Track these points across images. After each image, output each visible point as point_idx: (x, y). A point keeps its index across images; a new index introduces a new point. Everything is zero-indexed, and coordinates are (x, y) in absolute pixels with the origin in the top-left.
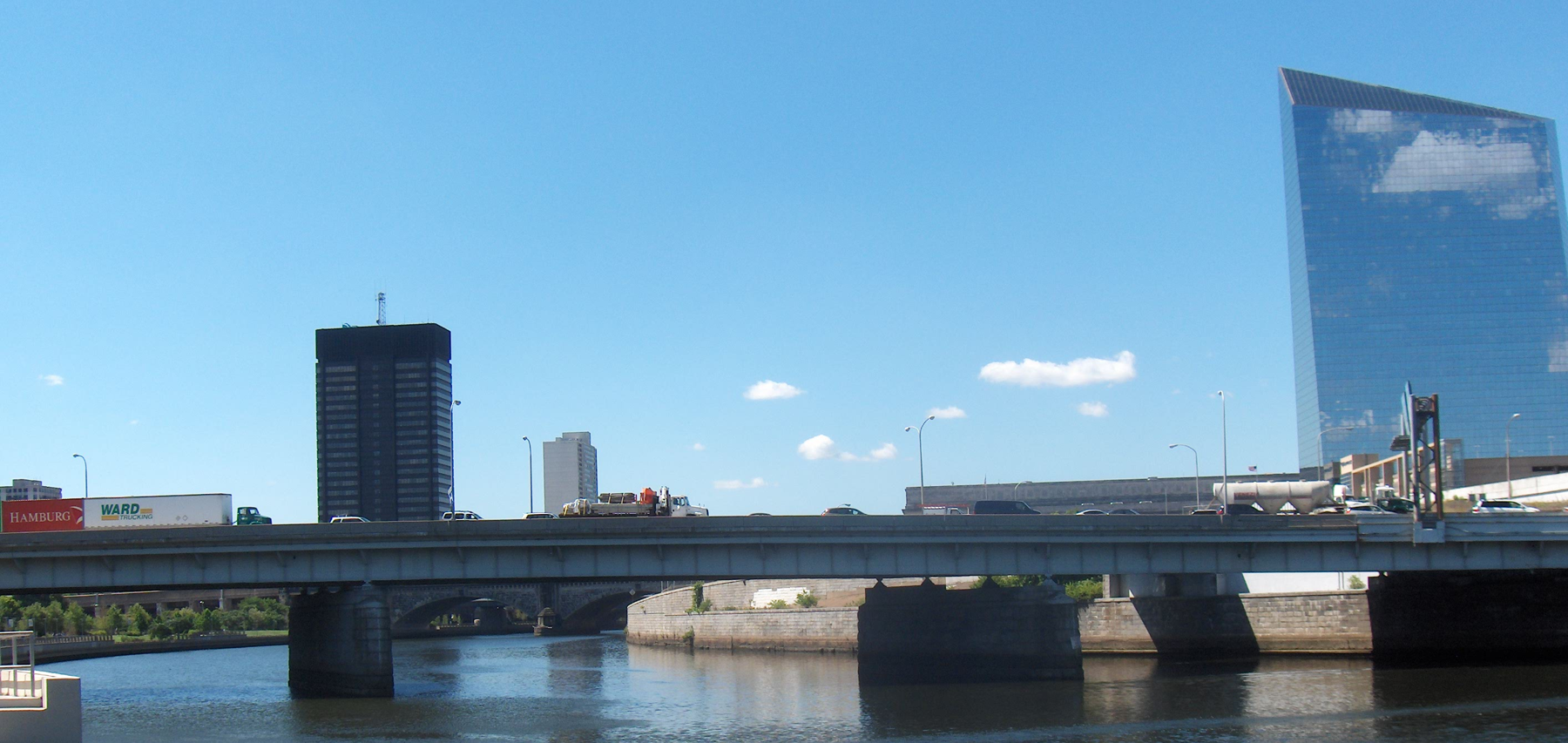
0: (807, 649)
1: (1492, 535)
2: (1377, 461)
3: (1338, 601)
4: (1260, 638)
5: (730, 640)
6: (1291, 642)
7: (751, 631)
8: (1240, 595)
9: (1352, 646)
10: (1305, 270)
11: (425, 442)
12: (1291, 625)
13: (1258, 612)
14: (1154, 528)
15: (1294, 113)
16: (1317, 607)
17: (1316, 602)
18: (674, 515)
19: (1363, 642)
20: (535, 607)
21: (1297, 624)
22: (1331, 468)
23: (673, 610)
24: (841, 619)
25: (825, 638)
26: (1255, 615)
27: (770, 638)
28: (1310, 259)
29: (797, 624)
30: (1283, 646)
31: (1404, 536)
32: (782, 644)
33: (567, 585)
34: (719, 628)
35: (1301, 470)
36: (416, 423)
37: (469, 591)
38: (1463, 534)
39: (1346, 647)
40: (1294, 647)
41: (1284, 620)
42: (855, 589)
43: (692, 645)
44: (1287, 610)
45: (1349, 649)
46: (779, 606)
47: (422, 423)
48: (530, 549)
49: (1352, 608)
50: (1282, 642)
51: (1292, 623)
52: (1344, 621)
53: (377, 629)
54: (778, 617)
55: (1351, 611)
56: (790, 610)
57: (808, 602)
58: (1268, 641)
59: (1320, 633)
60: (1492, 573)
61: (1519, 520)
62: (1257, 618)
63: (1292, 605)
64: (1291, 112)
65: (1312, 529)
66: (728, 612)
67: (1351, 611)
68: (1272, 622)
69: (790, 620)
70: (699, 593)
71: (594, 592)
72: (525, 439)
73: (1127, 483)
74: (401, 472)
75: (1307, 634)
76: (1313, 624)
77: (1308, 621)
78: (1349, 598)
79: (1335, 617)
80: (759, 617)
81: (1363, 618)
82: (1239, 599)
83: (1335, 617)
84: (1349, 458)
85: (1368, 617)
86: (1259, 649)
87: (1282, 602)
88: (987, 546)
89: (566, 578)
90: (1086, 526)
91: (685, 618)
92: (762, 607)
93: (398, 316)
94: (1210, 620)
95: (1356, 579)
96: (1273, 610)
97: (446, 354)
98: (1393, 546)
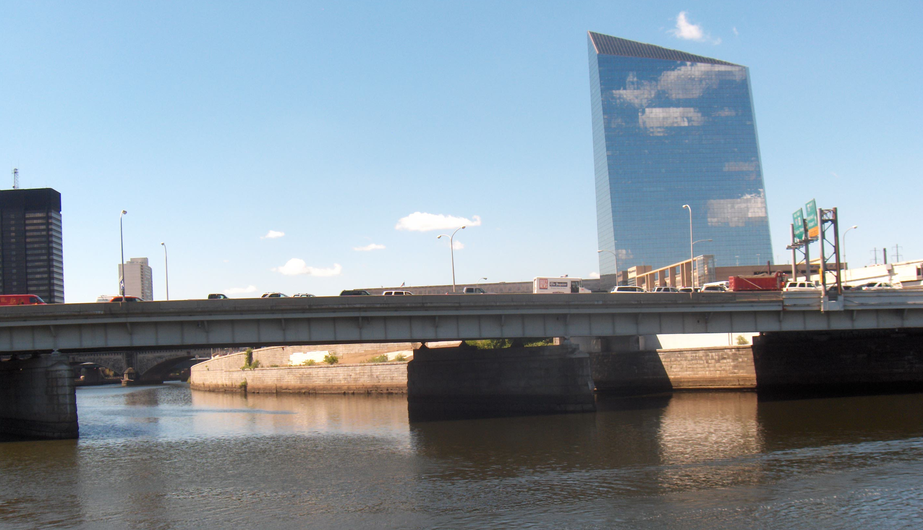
0: (333, 392)
1: (872, 305)
2: (651, 271)
3: (730, 353)
4: (673, 379)
5: (275, 387)
6: (695, 381)
7: (290, 380)
8: (657, 350)
9: (741, 383)
10: (606, 154)
11: (45, 263)
12: (695, 370)
13: (670, 361)
14: (644, 302)
15: (598, 58)
16: (715, 357)
17: (714, 354)
18: (281, 297)
19: (750, 380)
20: (121, 367)
22: (621, 275)
23: (230, 367)
24: (358, 372)
25: (347, 384)
26: (669, 363)
27: (305, 385)
28: (608, 148)
29: (325, 375)
30: (690, 384)
31: (814, 306)
32: (314, 389)
33: (143, 353)
34: (266, 379)
35: (601, 276)
36: (39, 252)
37: (78, 358)
38: (854, 305)
39: (737, 384)
40: (698, 384)
41: (690, 366)
42: (363, 352)
43: (245, 390)
44: (692, 360)
46: (311, 364)
47: (44, 251)
48: (182, 323)
49: (741, 357)
50: (689, 382)
51: (697, 368)
52: (735, 367)
53: (65, 386)
54: (310, 371)
55: (740, 360)
56: (319, 366)
57: (332, 361)
58: (679, 381)
59: (718, 374)
60: (892, 331)
61: (891, 294)
62: (670, 366)
63: (696, 356)
64: (596, 58)
66: (273, 368)
67: (740, 360)
68: (682, 368)
69: (320, 373)
70: (250, 357)
71: (160, 357)
72: (163, 244)
73: (488, 286)
74: (30, 283)
75: (708, 375)
76: (712, 369)
77: (708, 367)
78: (739, 351)
79: (728, 364)
80: (297, 371)
81: (749, 364)
82: (656, 353)
83: (728, 364)
84: (634, 268)
85: (753, 364)
86: (672, 386)
87: (689, 355)
88: (523, 316)
89: (261, 343)
90: (598, 301)
91: (240, 373)
92: (298, 364)
93: (27, 183)
94: (635, 367)
95: (741, 339)
96: (681, 360)
97: (59, 209)
98: (804, 313)
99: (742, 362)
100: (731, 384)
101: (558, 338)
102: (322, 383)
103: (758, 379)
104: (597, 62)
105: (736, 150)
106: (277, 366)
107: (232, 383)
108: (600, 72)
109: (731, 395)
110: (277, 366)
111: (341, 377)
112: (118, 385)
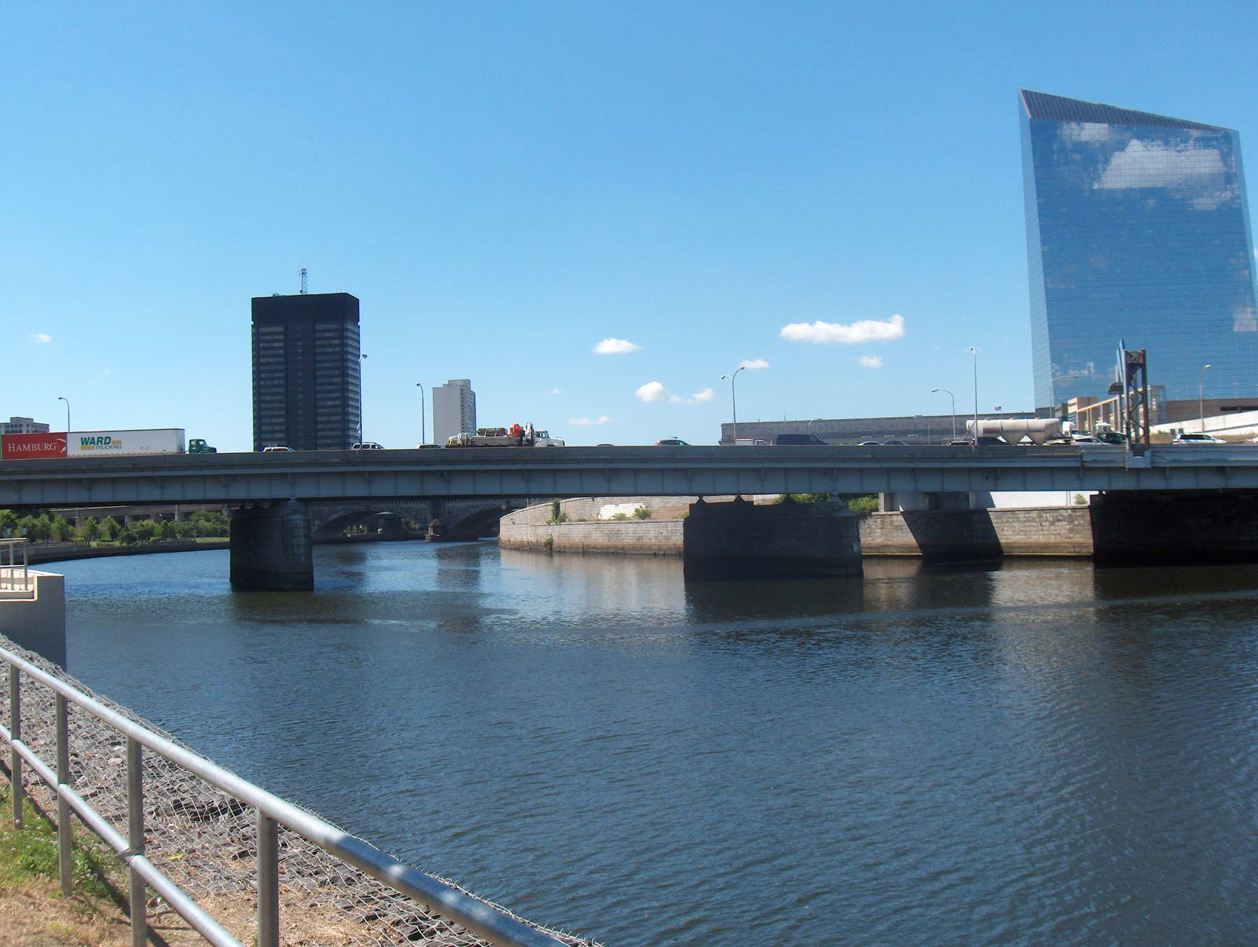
0: (643, 552)
1: (1188, 462)
3: (1066, 514)
4: (1004, 543)
6: (1028, 547)
7: (598, 538)
9: (1077, 550)
10: (1040, 250)
11: (339, 387)
12: (1029, 533)
13: (1002, 523)
17: (1048, 515)
19: (1086, 547)
21: (1033, 533)
22: (1060, 408)
24: (670, 529)
25: (657, 543)
26: (1000, 525)
28: (1043, 242)
29: (635, 532)
30: (1022, 550)
32: (623, 548)
33: (452, 501)
35: (1036, 410)
36: (331, 372)
37: (374, 506)
38: (1166, 460)
40: (1031, 551)
41: (1023, 529)
43: (551, 549)
44: (1025, 522)
45: (1075, 552)
46: (621, 518)
47: (337, 372)
49: (1077, 520)
50: (1021, 547)
51: (1029, 531)
52: (1071, 530)
53: (300, 536)
54: (620, 527)
55: (1076, 522)
57: (643, 515)
58: (1011, 546)
59: (1052, 539)
61: (1210, 450)
63: (1029, 517)
64: (1028, 124)
65: (1045, 457)
67: (1076, 522)
68: (1014, 531)
70: (557, 508)
72: (418, 385)
73: (898, 420)
76: (1046, 532)
77: (1042, 530)
79: (1063, 526)
81: (1086, 528)
82: (987, 512)
83: (1063, 526)
84: (1075, 400)
85: (1090, 527)
86: (1003, 552)
87: (1021, 515)
88: (786, 470)
90: (866, 454)
91: (545, 528)
92: (607, 519)
93: (317, 287)
94: (964, 529)
95: (1080, 497)
96: (1014, 522)
99: (1079, 525)
100: (1066, 551)
101: (883, 494)
102: (631, 542)
103: (1095, 545)
104: (1029, 130)
105: (1217, 242)
106: (585, 521)
107: (537, 539)
108: (1033, 142)
109: (896, 561)
110: (585, 521)
111: (652, 535)
112: (423, 541)
